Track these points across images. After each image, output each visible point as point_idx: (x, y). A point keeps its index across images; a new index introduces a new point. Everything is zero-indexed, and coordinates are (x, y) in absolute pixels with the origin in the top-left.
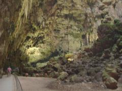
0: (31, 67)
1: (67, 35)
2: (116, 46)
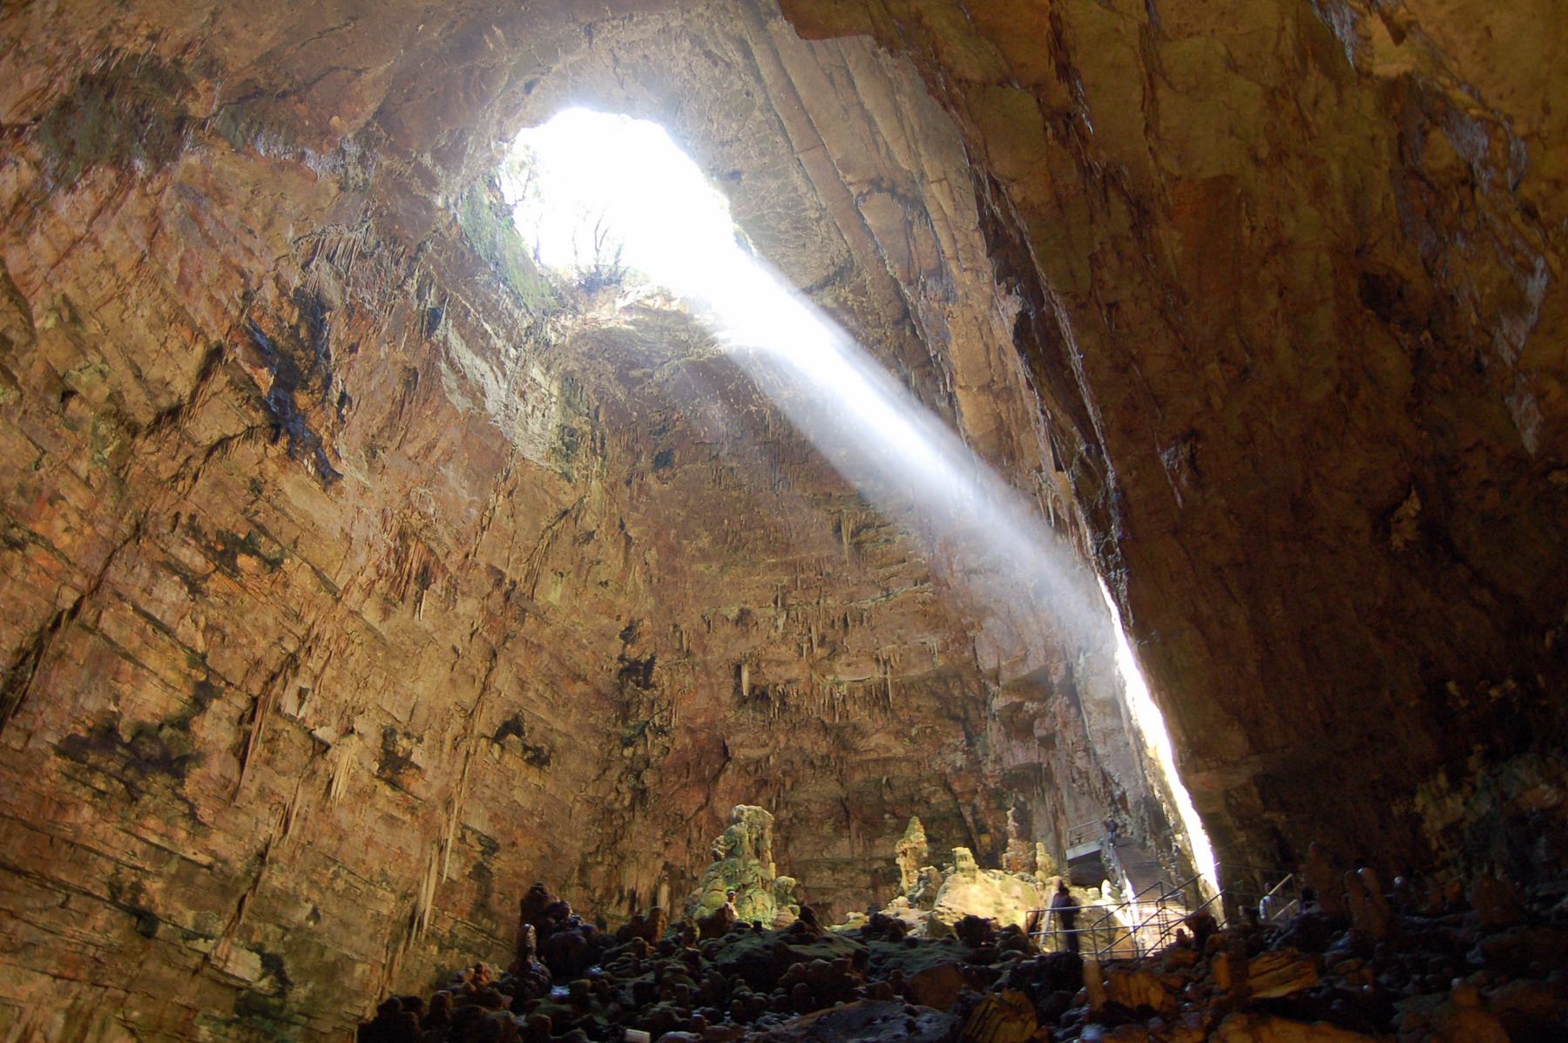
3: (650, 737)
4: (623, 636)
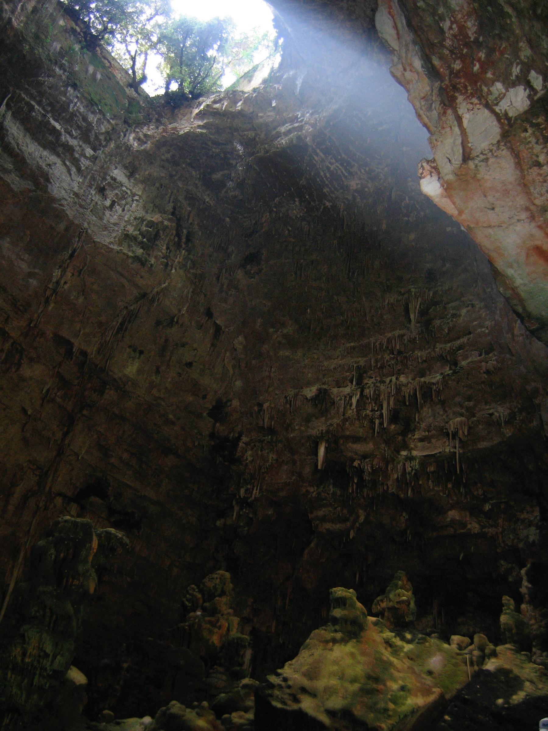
4: (211, 414)
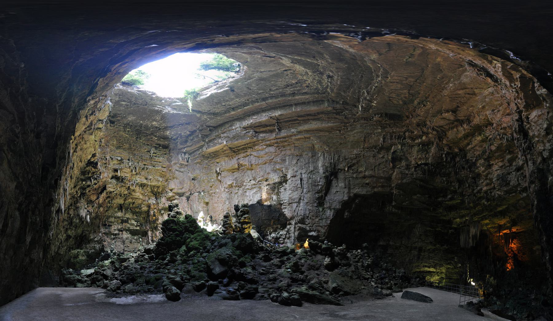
0: (74, 275)
1: (122, 231)
2: (184, 248)
3: (92, 180)
